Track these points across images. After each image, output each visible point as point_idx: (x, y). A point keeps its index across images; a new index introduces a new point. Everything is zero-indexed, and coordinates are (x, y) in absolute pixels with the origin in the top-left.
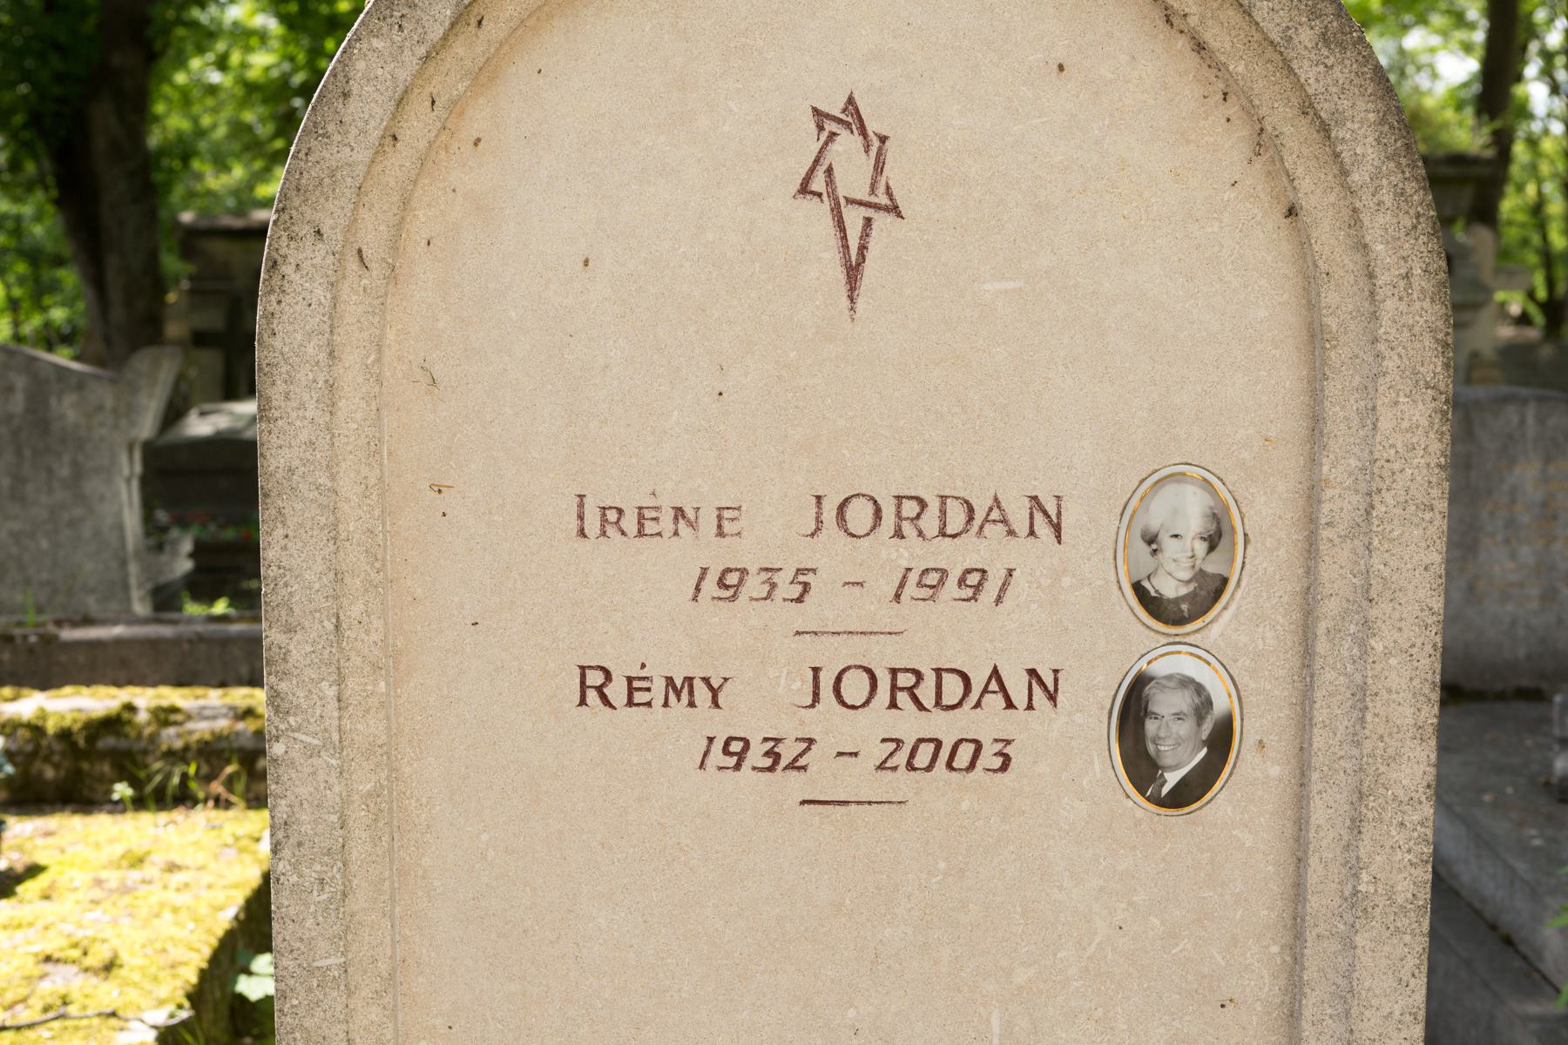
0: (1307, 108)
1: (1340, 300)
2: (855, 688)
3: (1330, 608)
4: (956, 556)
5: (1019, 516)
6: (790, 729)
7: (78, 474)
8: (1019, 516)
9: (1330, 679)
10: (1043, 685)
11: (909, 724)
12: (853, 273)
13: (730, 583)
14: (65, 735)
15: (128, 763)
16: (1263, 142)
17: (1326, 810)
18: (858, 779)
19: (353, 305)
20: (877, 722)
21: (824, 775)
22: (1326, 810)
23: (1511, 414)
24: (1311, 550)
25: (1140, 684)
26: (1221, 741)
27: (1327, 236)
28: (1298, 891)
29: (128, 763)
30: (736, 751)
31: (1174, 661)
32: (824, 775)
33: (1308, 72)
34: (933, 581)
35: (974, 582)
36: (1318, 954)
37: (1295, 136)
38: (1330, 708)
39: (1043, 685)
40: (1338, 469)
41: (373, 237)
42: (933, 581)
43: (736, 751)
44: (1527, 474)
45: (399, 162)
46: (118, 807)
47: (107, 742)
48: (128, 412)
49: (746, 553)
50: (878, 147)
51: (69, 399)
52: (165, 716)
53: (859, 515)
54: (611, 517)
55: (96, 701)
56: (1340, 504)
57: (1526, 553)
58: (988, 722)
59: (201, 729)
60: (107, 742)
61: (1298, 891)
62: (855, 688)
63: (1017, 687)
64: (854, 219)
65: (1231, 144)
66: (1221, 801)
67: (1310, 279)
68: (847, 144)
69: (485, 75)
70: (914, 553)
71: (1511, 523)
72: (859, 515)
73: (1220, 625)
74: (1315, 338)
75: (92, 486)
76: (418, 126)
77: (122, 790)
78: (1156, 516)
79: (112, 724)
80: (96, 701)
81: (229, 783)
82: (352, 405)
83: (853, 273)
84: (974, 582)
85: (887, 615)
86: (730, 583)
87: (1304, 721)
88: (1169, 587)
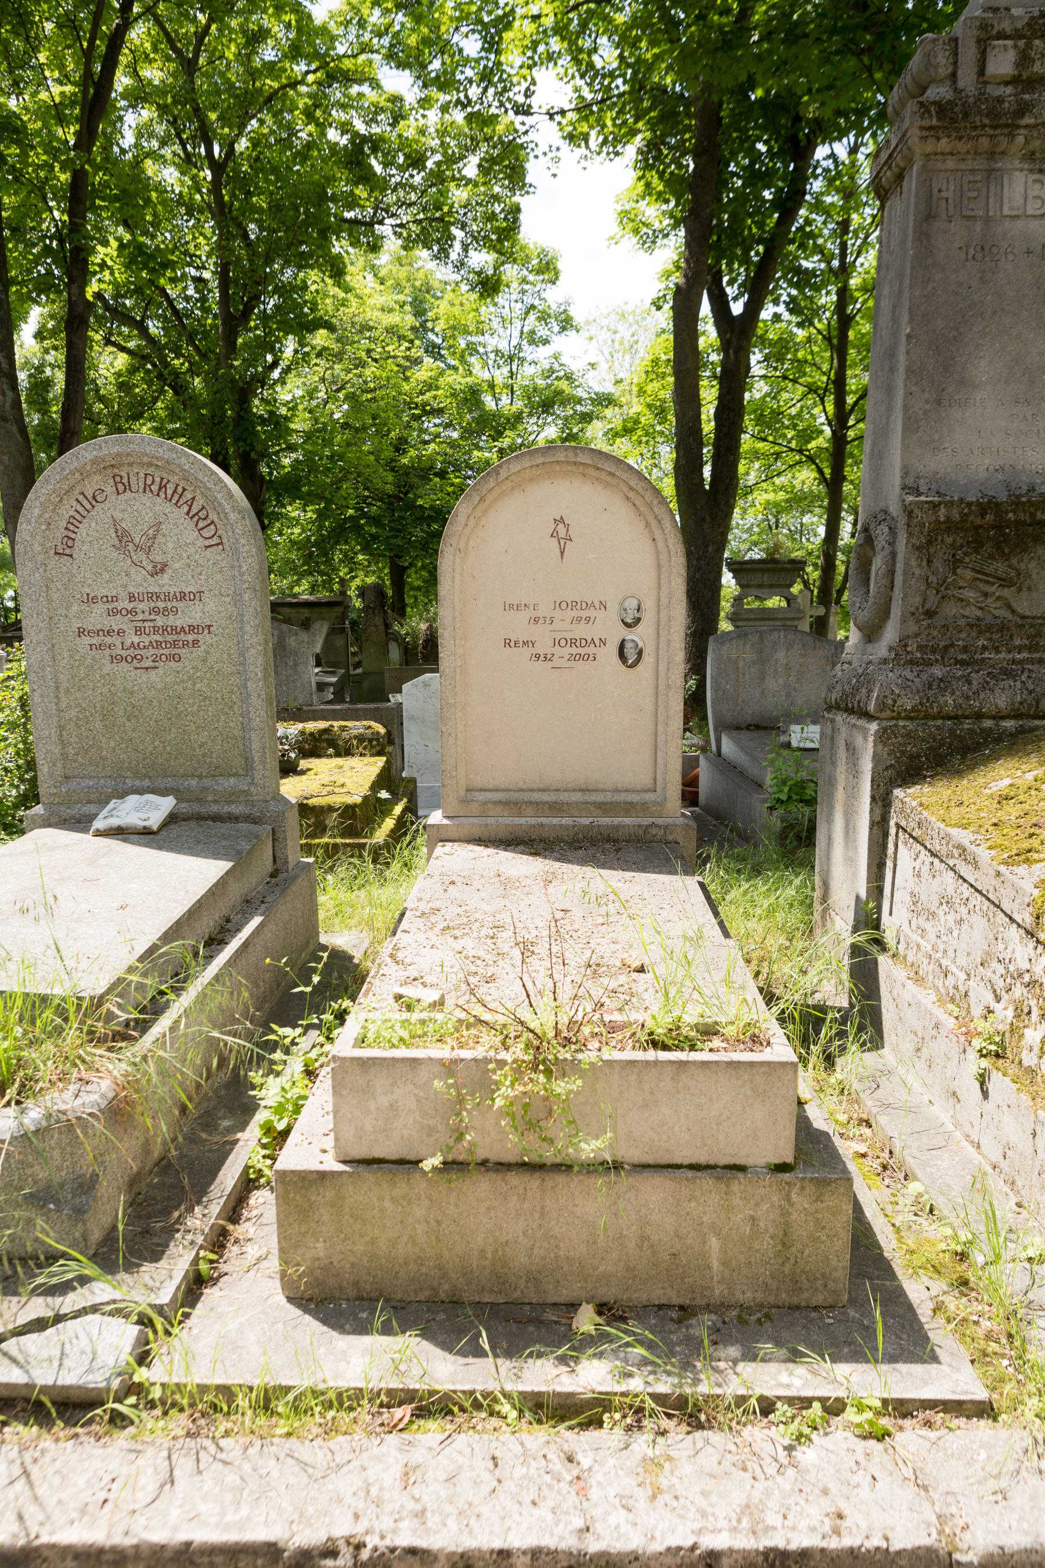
0: (656, 517)
1: (663, 558)
2: (563, 643)
3: (662, 623)
4: (584, 614)
5: (597, 606)
6: (549, 652)
7: (296, 664)
8: (597, 606)
9: (663, 639)
10: (603, 642)
11: (574, 650)
12: (562, 553)
13: (536, 620)
14: (312, 734)
15: (332, 743)
16: (647, 525)
17: (662, 667)
18: (563, 663)
19: (458, 561)
20: (568, 650)
21: (556, 662)
22: (662, 667)
23: (776, 634)
24: (659, 612)
25: (624, 640)
26: (640, 653)
27: (661, 544)
28: (657, 686)
29: (332, 743)
30: (538, 657)
31: (630, 635)
32: (556, 662)
33: (656, 510)
34: (579, 620)
35: (588, 620)
36: (661, 699)
37: (654, 523)
38: (663, 645)
39: (603, 642)
40: (664, 594)
41: (462, 546)
42: (579, 620)
43: (538, 657)
44: (781, 655)
45: (467, 530)
46: (330, 756)
47: (325, 736)
48: (313, 643)
49: (540, 614)
50: (567, 527)
51: (293, 638)
52: (343, 729)
53: (564, 605)
54: (511, 606)
55: (322, 725)
56: (664, 601)
57: (781, 681)
58: (591, 650)
59: (355, 732)
60: (325, 736)
61: (657, 686)
62: (563, 643)
63: (597, 642)
64: (562, 542)
65: (641, 525)
66: (641, 667)
67: (658, 554)
68: (561, 525)
69: (485, 512)
70: (574, 614)
71: (775, 671)
72: (564, 605)
73: (640, 628)
74: (659, 566)
75: (300, 668)
76: (472, 522)
77: (331, 751)
78: (626, 605)
79: (326, 731)
80: (322, 725)
81: (365, 748)
82: (457, 581)
83: (562, 553)
84: (588, 620)
85: (569, 627)
86: (536, 620)
87: (658, 649)
88: (629, 621)
